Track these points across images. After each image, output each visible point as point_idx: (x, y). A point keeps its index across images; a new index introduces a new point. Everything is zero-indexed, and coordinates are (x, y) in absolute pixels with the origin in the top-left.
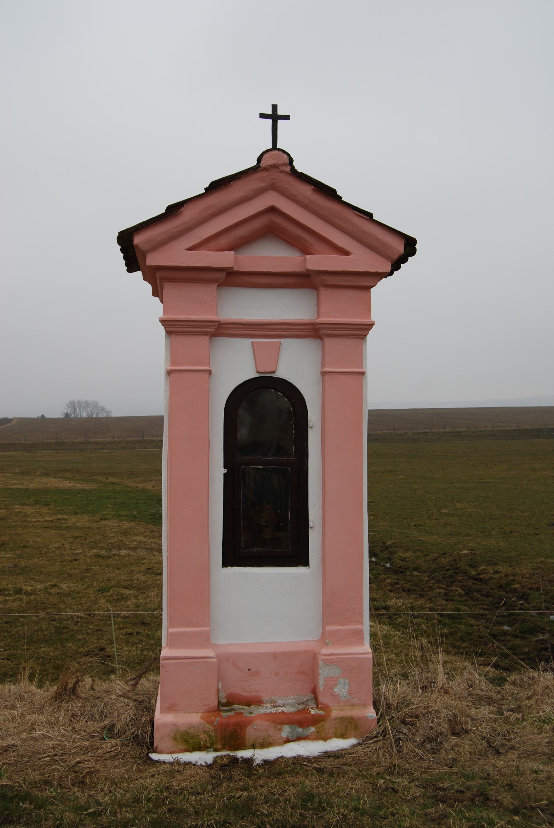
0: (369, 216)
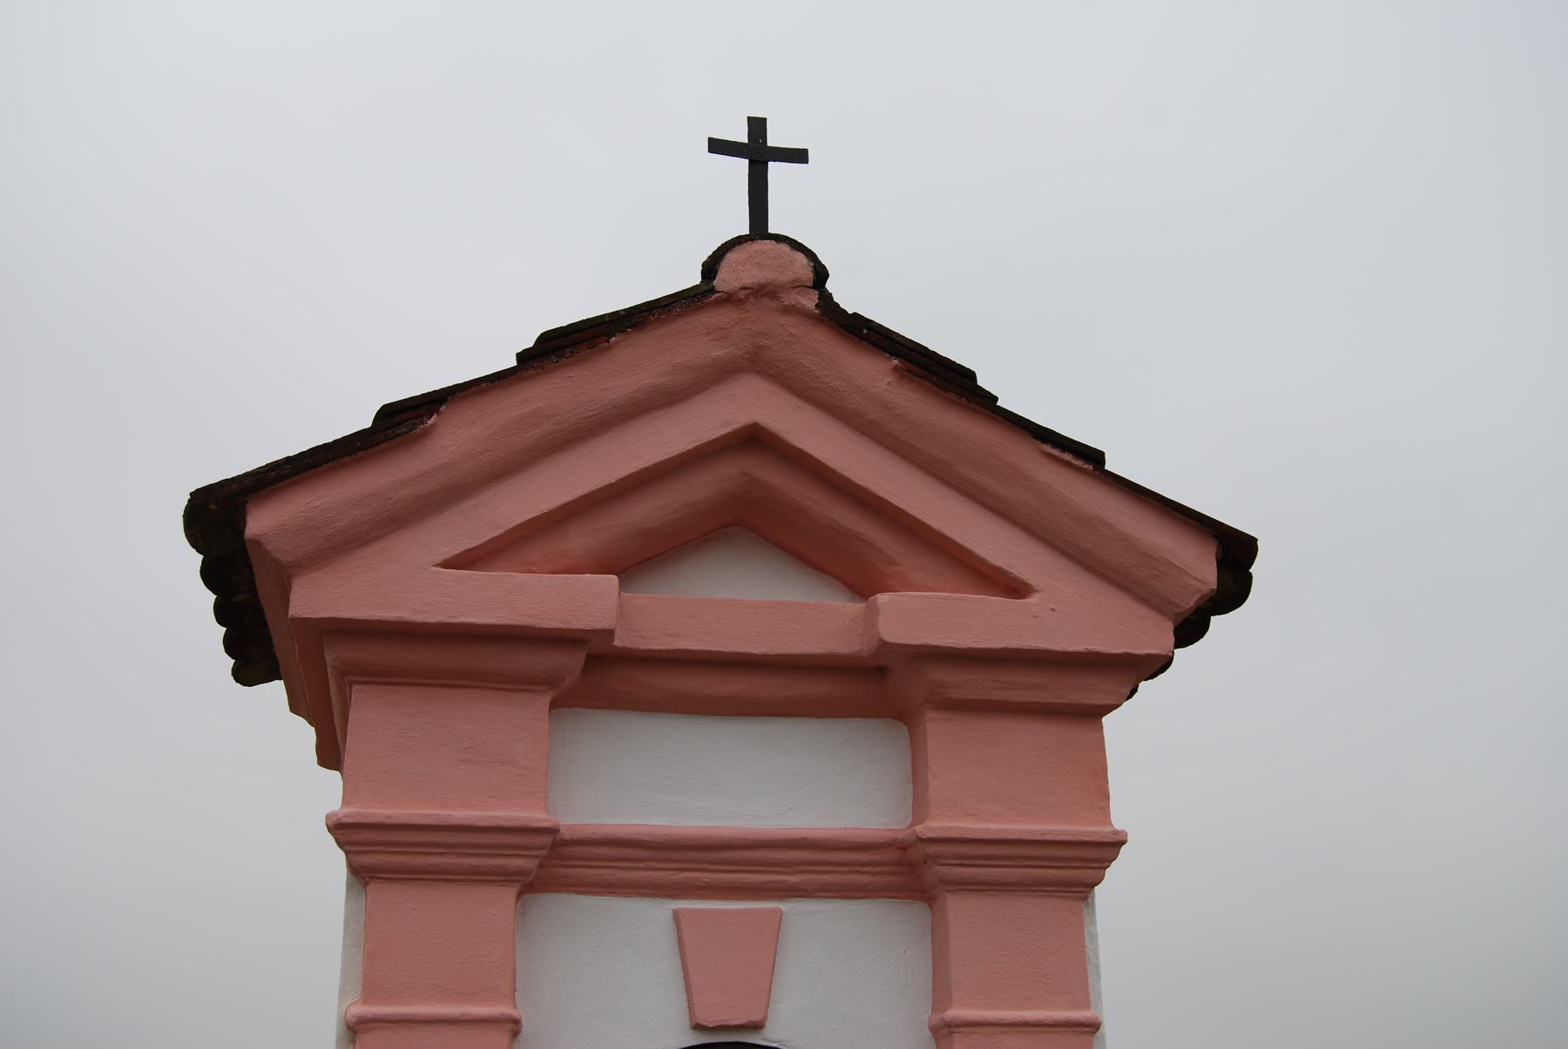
0: (1094, 457)
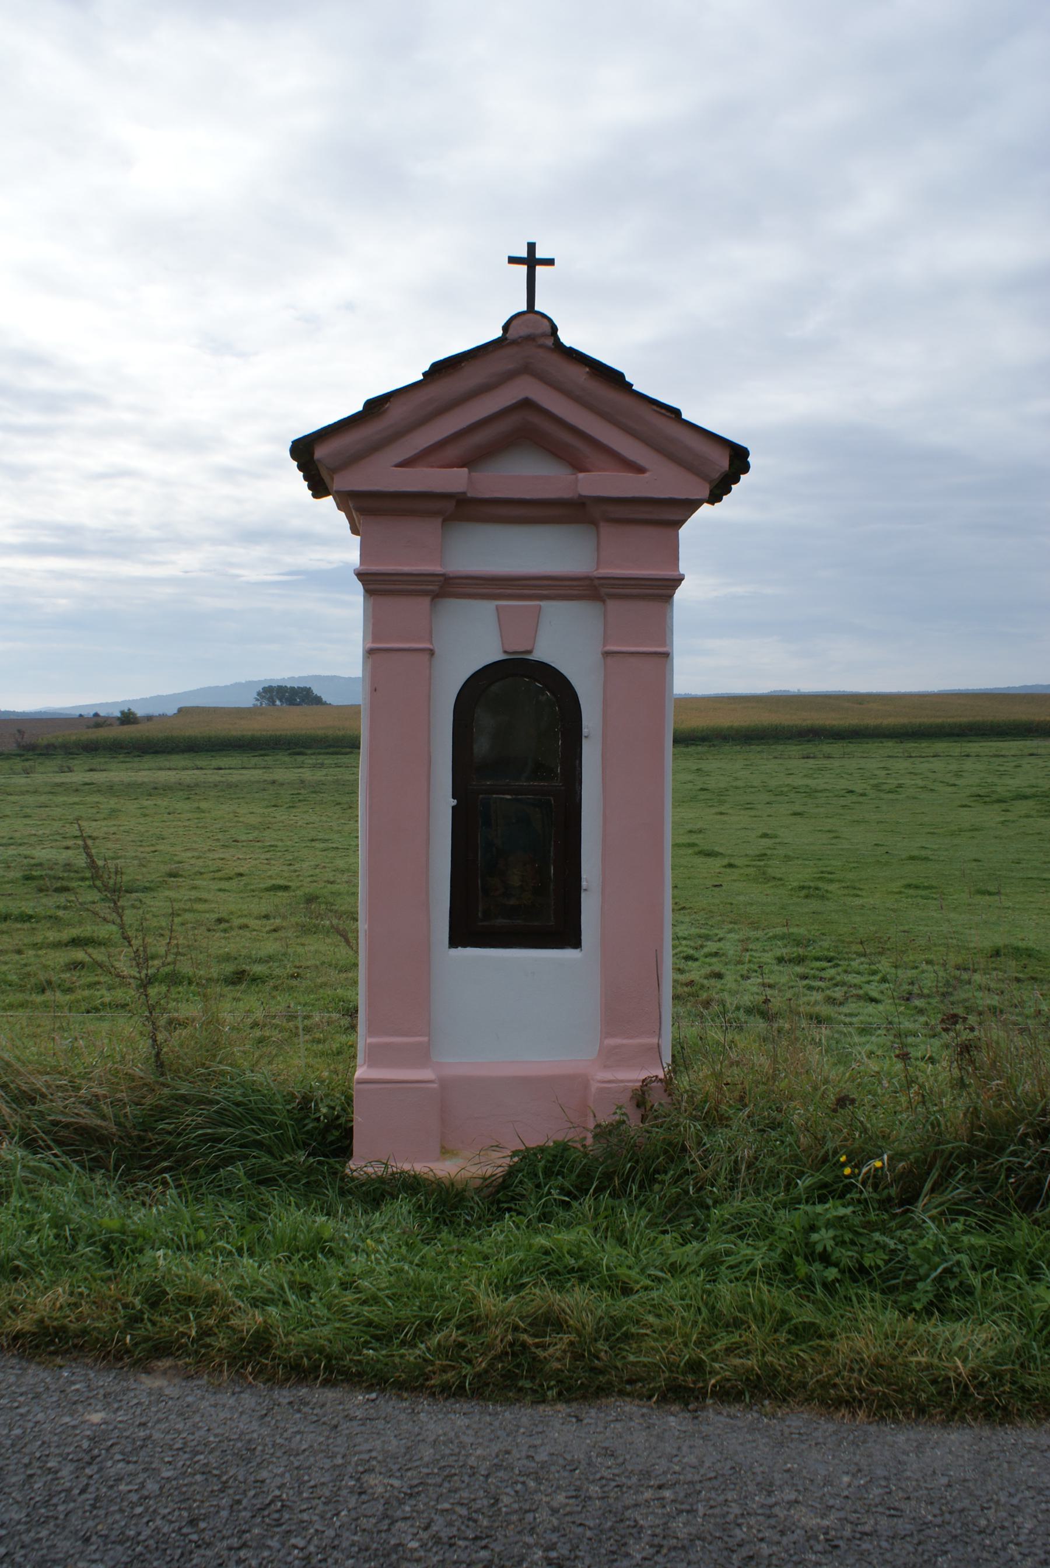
0: (676, 412)
